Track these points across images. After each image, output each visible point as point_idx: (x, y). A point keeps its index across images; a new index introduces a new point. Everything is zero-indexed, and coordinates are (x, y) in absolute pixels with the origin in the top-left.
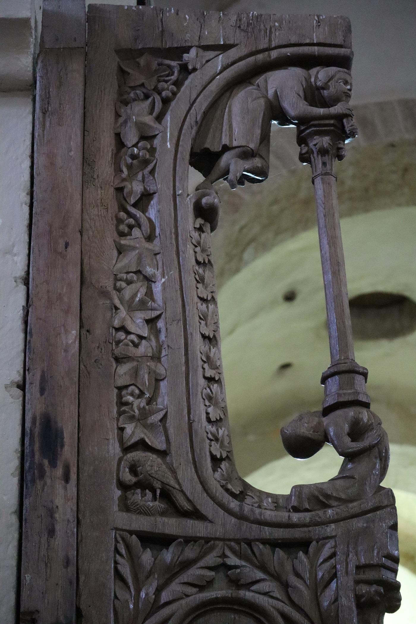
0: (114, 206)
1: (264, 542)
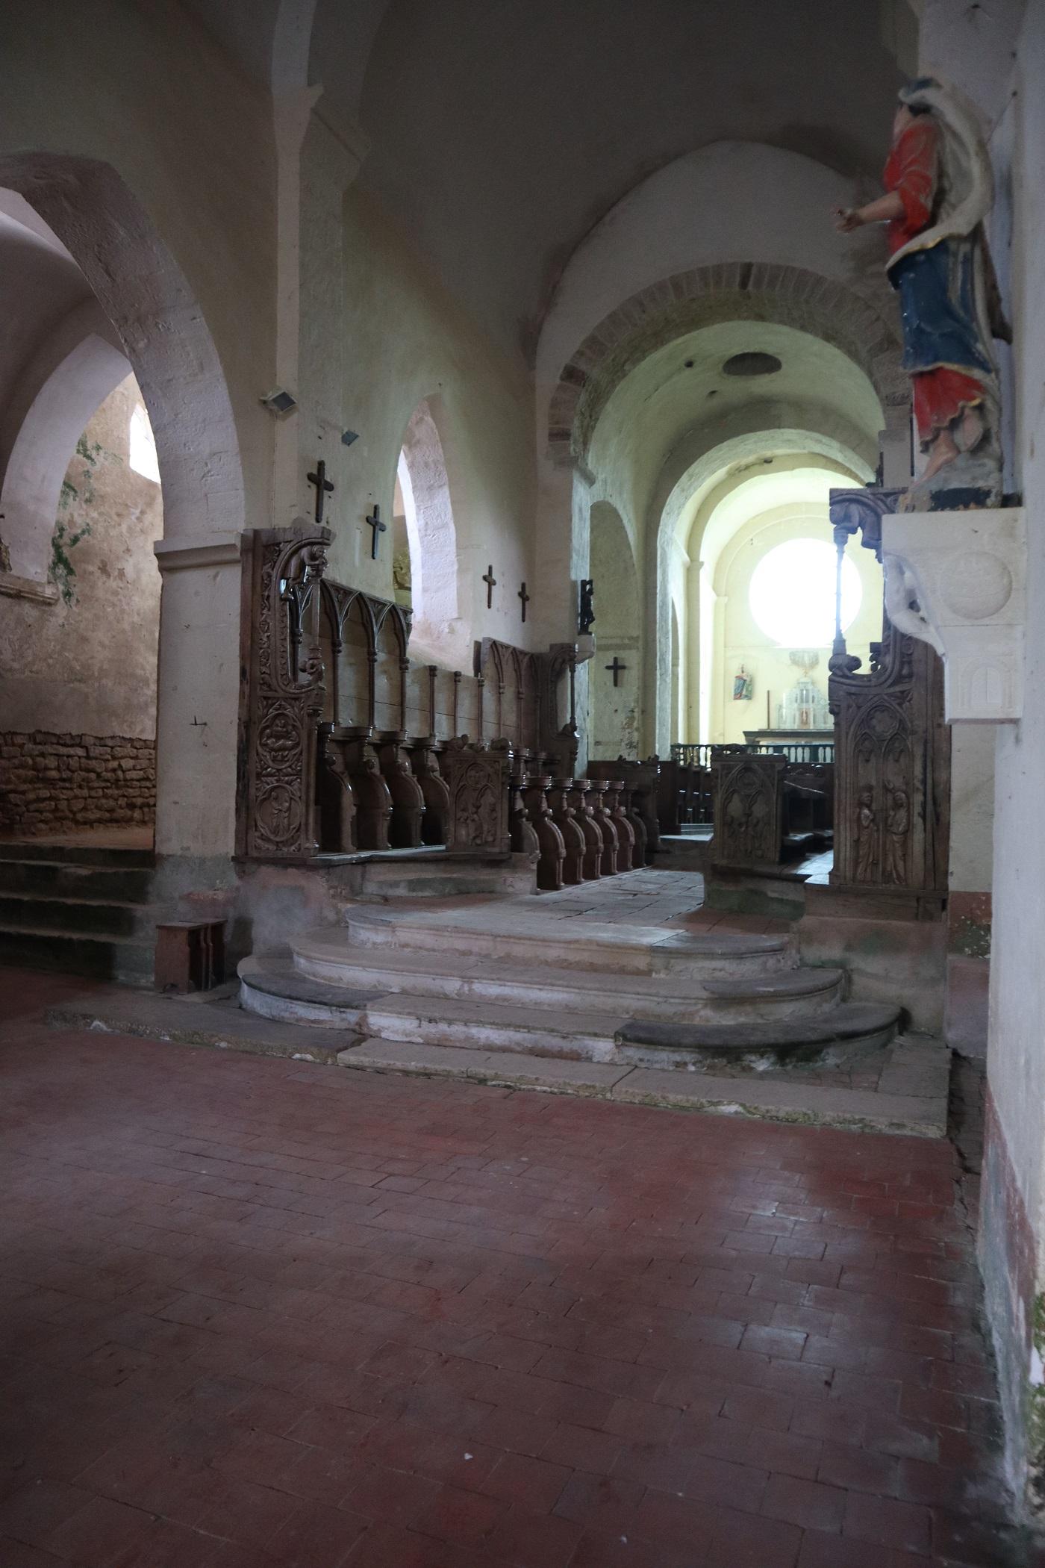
0: (261, 600)
1: (290, 698)
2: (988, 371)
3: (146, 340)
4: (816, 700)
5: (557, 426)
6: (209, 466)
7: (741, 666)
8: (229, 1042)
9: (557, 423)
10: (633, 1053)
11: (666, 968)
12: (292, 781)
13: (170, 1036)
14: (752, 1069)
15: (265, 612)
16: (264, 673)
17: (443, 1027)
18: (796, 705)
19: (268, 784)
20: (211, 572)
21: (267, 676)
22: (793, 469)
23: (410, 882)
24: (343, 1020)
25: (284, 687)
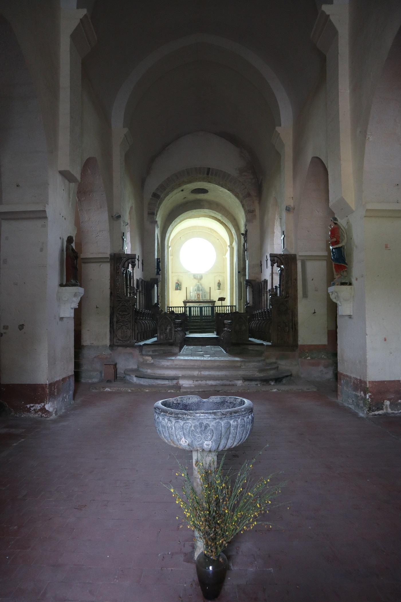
2: (347, 265)
3: (85, 198)
4: (202, 290)
5: (150, 211)
6: (99, 234)
7: (177, 279)
8: (149, 390)
9: (151, 210)
10: (246, 383)
11: (245, 365)
12: (128, 324)
13: (131, 390)
14: (271, 384)
15: (118, 276)
16: (118, 294)
17: (200, 382)
18: (196, 292)
19: (120, 324)
20: (99, 264)
21: (119, 295)
22: (199, 217)
23: (152, 351)
24: (172, 383)
25: (124, 298)
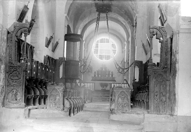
25: (16, 64)
